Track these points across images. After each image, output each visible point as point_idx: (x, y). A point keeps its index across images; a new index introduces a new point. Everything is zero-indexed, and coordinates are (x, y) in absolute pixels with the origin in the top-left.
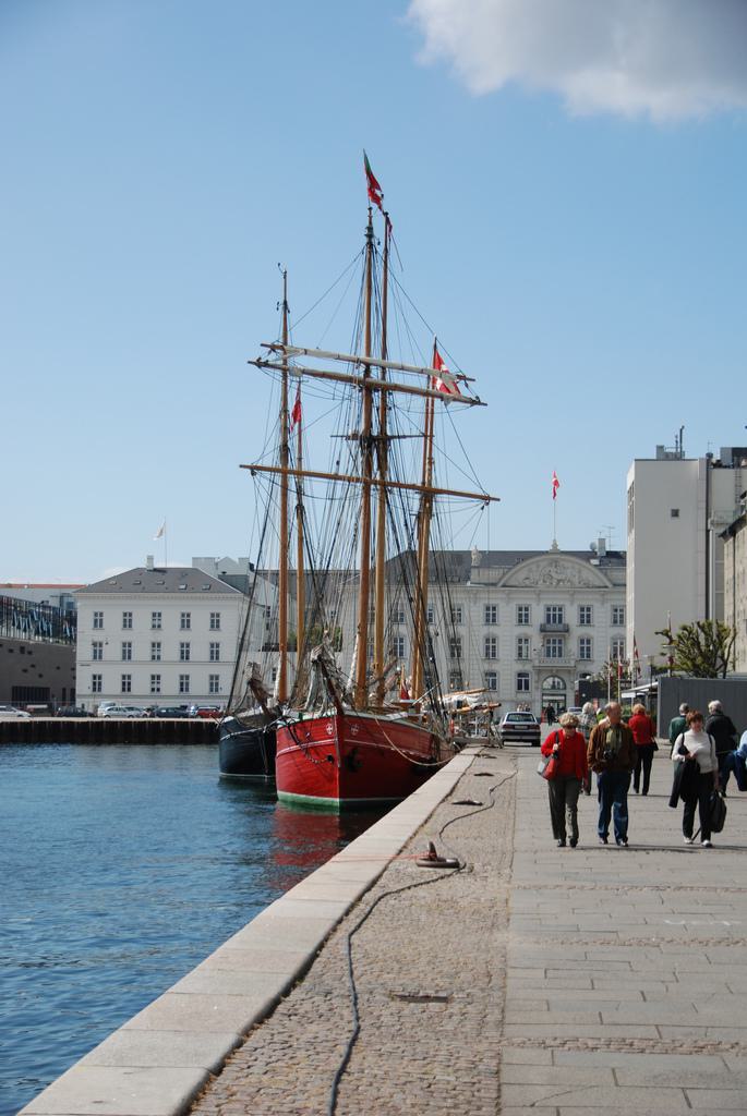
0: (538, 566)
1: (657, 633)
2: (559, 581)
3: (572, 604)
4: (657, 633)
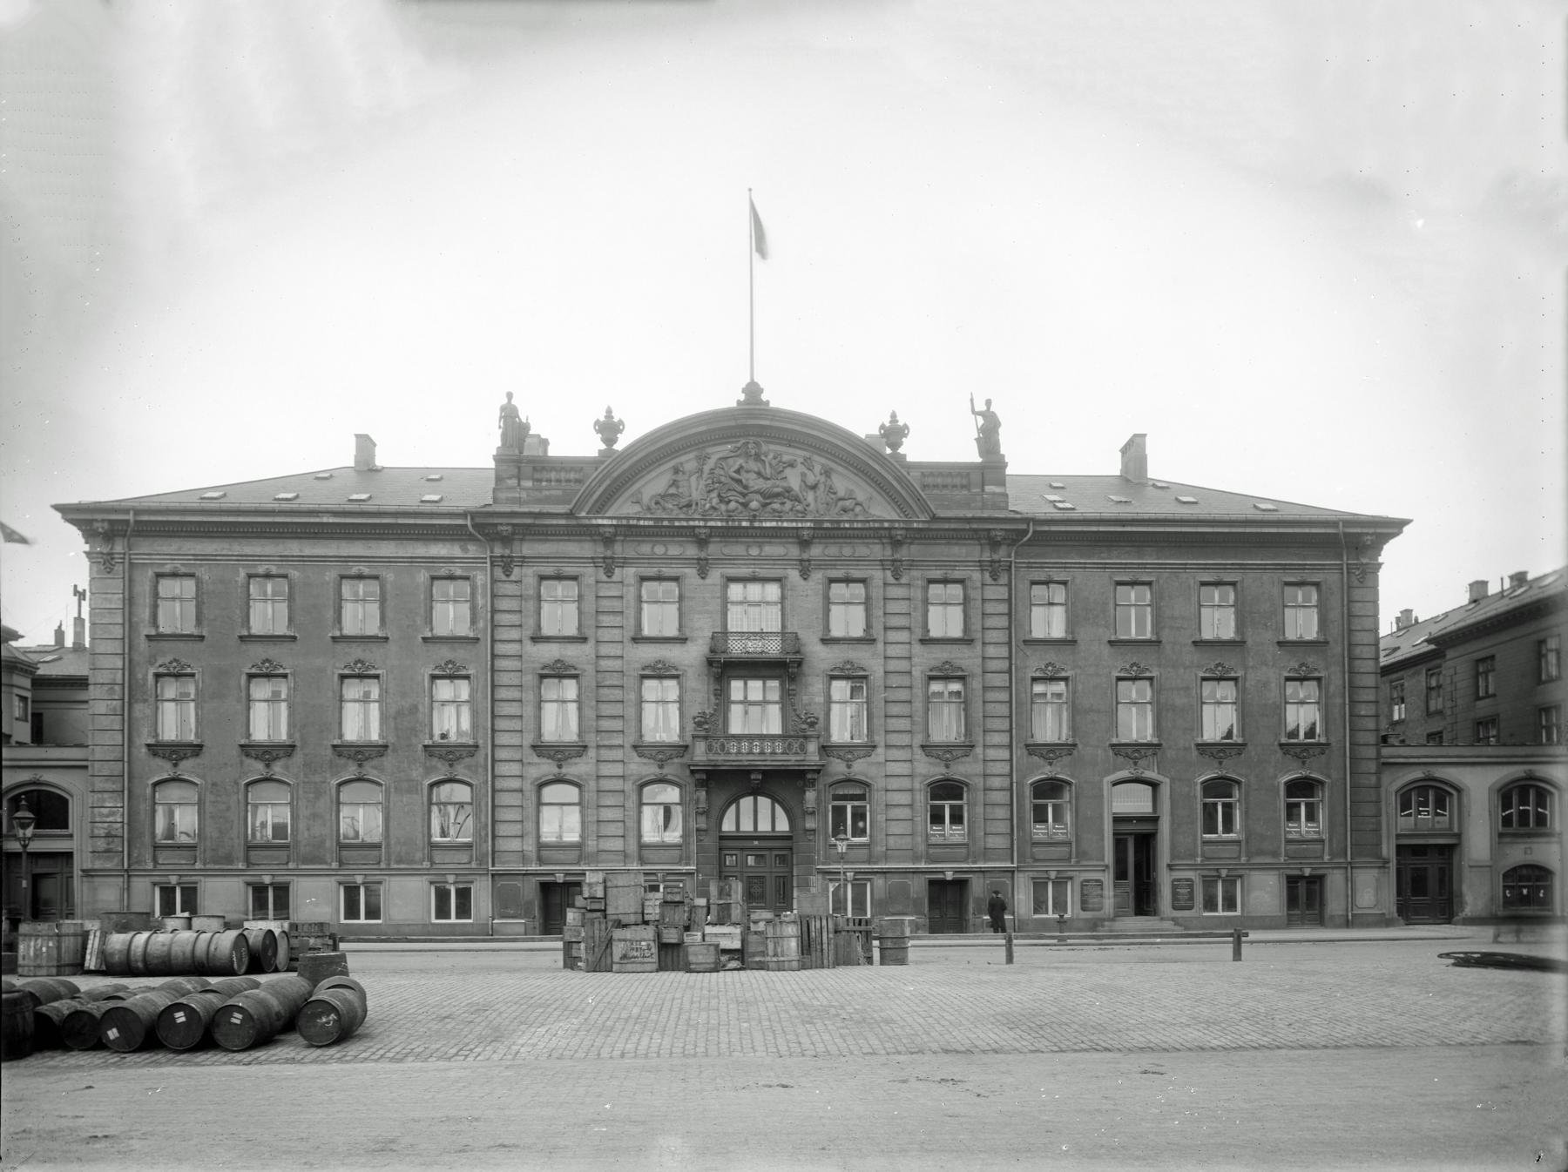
0: (703, 459)
1: (510, 396)
2: (768, 497)
3: (703, 574)
4: (510, 396)
